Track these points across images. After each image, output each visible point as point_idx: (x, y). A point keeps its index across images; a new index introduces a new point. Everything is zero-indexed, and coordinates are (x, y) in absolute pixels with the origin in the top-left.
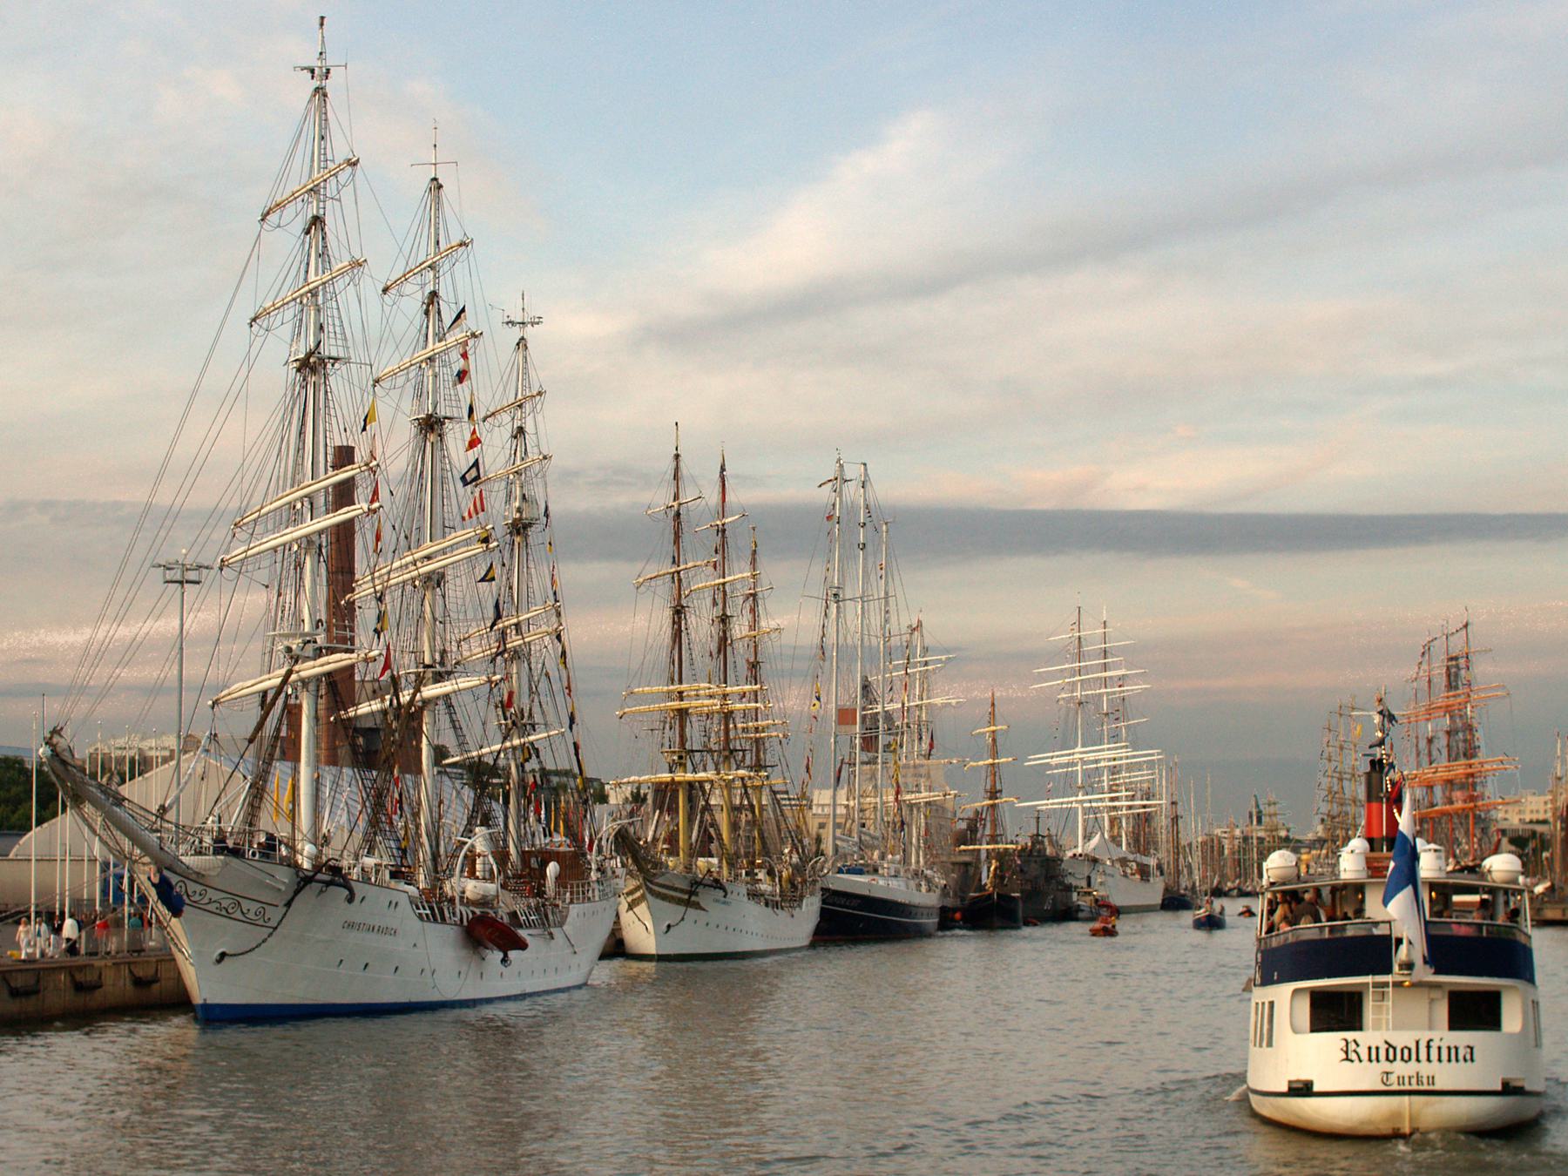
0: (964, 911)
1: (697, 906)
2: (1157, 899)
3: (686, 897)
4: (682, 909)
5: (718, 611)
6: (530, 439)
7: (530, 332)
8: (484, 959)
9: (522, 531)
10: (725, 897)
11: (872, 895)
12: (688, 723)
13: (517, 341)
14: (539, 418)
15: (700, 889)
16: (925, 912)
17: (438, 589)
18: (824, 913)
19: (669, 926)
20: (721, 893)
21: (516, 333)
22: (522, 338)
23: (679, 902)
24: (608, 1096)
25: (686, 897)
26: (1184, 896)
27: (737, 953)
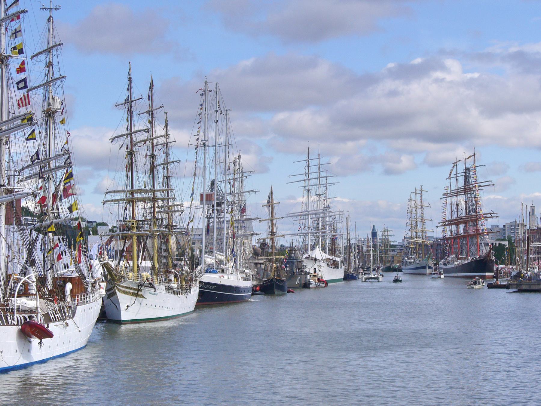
0: (261, 286)
1: (142, 296)
2: (342, 276)
3: (136, 292)
4: (134, 298)
5: (149, 153)
6: (56, 68)
7: (54, 13)
8: (30, 342)
9: (52, 115)
10: (155, 291)
11: (221, 284)
12: (136, 207)
13: (48, 18)
14: (60, 56)
15: (143, 288)
16: (246, 290)
17: (7, 145)
18: (201, 293)
19: (128, 306)
20: (154, 290)
21: (47, 14)
22: (50, 17)
23: (133, 294)
24: (125, 203)
25: (136, 292)
26: (353, 274)
27: (161, 318)
